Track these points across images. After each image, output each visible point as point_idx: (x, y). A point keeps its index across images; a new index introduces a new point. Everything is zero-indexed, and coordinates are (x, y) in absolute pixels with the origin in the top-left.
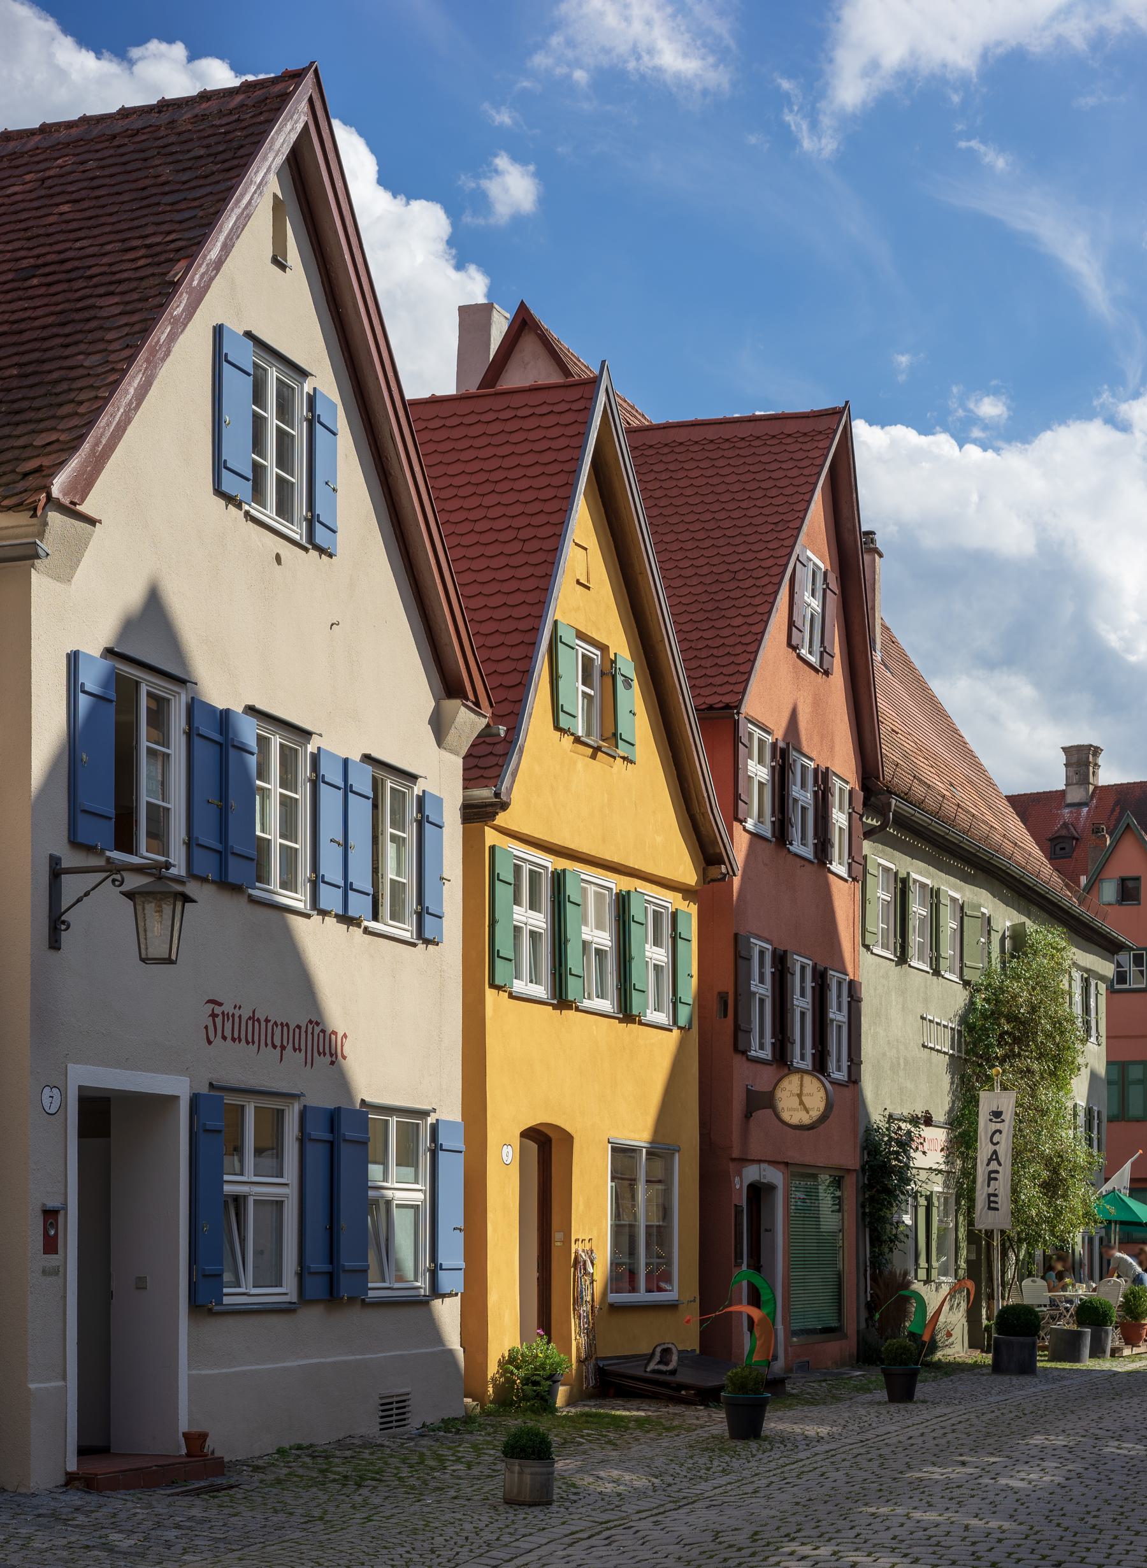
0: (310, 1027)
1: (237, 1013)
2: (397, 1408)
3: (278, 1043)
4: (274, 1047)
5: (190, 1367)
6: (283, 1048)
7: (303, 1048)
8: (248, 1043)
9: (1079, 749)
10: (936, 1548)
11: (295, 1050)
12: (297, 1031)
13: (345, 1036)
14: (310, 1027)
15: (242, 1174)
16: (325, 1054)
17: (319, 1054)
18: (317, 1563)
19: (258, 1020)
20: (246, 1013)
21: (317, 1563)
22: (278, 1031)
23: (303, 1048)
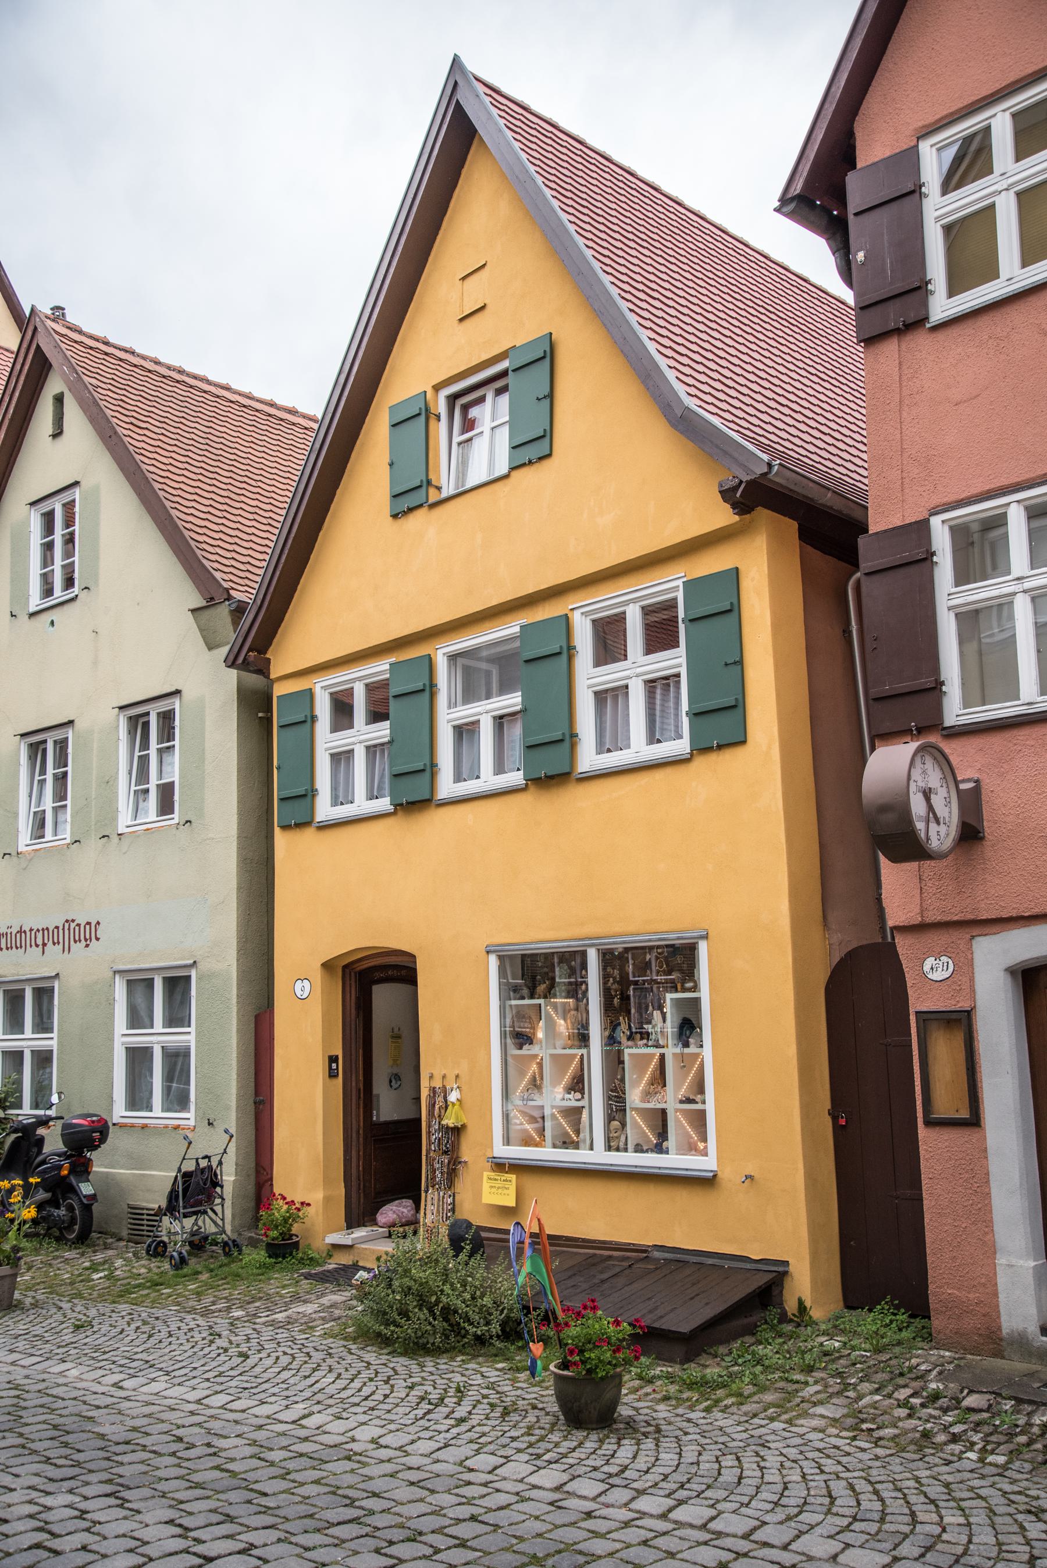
0: (67, 925)
1: (9, 931)
2: (148, 1226)
3: (40, 941)
4: (37, 946)
5: (697, 1001)
6: (44, 945)
7: (61, 940)
8: (17, 948)
9: (164, 713)
10: (12, 1368)
11: (54, 944)
12: (88, 927)
13: (98, 923)
14: (67, 925)
15: (152, 1027)
16: (80, 941)
17: (75, 942)
18: (154, 1452)
19: (25, 932)
20: (14, 930)
21: (154, 1452)
22: (40, 935)
23: (61, 940)
